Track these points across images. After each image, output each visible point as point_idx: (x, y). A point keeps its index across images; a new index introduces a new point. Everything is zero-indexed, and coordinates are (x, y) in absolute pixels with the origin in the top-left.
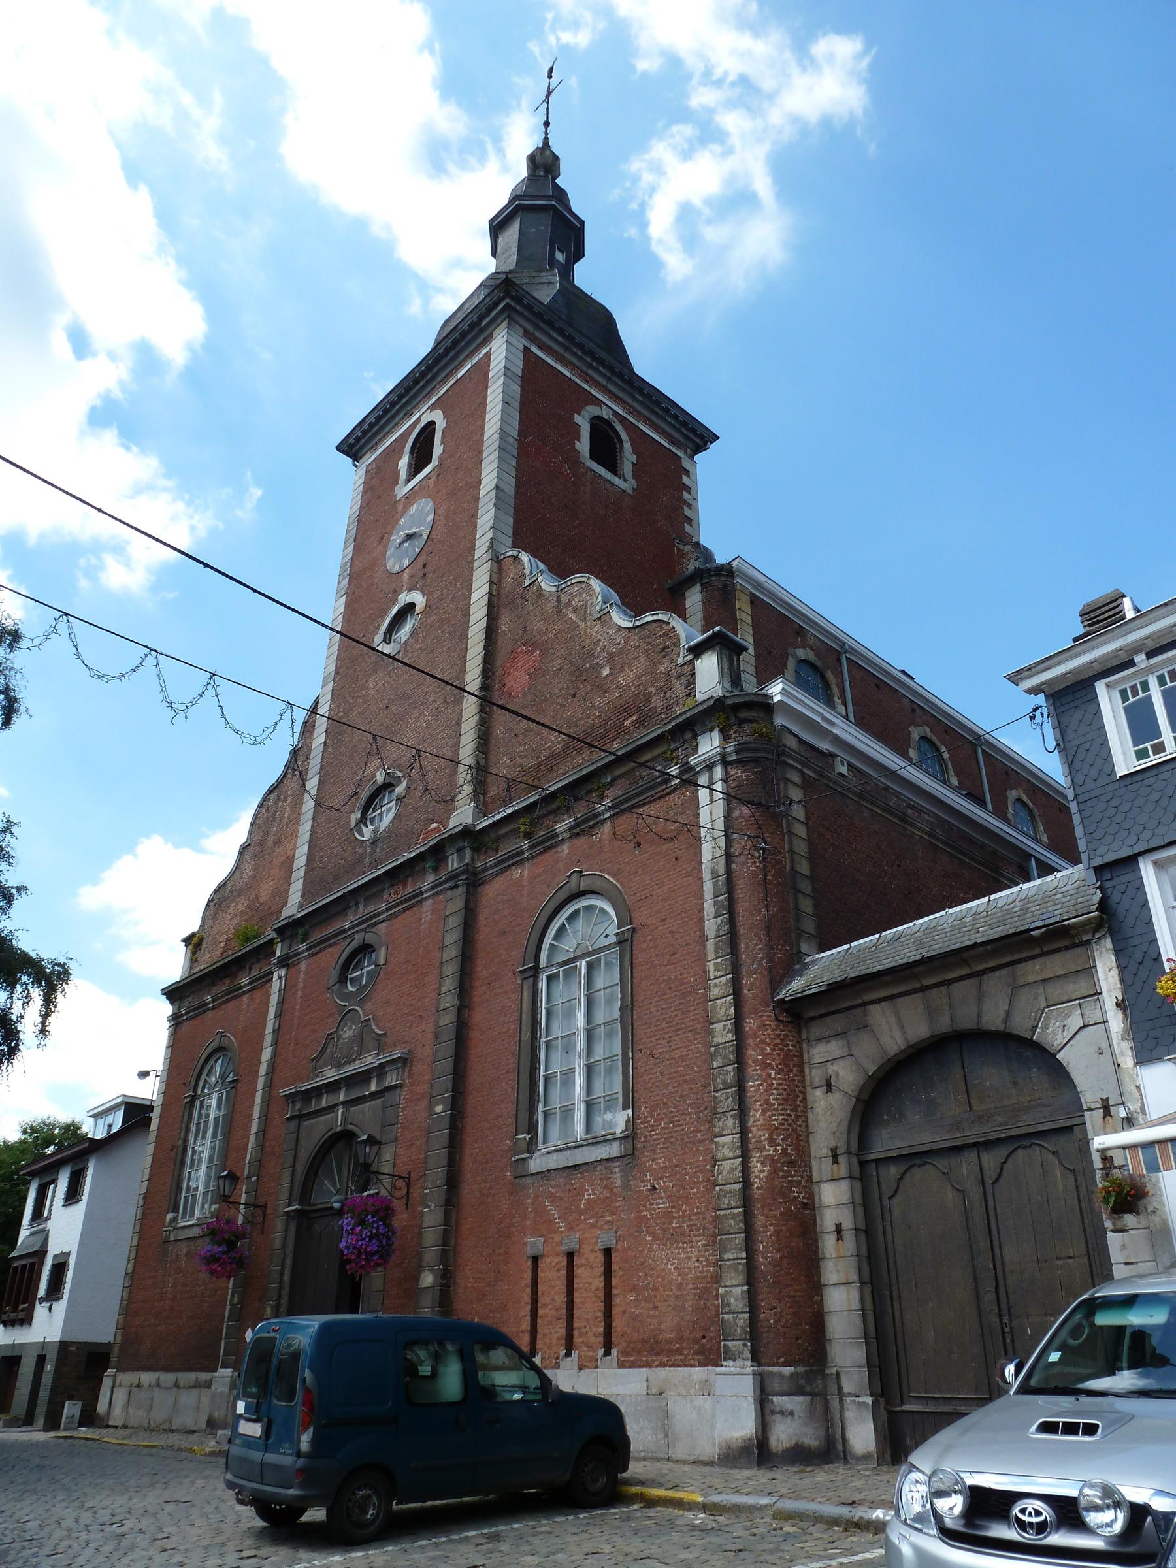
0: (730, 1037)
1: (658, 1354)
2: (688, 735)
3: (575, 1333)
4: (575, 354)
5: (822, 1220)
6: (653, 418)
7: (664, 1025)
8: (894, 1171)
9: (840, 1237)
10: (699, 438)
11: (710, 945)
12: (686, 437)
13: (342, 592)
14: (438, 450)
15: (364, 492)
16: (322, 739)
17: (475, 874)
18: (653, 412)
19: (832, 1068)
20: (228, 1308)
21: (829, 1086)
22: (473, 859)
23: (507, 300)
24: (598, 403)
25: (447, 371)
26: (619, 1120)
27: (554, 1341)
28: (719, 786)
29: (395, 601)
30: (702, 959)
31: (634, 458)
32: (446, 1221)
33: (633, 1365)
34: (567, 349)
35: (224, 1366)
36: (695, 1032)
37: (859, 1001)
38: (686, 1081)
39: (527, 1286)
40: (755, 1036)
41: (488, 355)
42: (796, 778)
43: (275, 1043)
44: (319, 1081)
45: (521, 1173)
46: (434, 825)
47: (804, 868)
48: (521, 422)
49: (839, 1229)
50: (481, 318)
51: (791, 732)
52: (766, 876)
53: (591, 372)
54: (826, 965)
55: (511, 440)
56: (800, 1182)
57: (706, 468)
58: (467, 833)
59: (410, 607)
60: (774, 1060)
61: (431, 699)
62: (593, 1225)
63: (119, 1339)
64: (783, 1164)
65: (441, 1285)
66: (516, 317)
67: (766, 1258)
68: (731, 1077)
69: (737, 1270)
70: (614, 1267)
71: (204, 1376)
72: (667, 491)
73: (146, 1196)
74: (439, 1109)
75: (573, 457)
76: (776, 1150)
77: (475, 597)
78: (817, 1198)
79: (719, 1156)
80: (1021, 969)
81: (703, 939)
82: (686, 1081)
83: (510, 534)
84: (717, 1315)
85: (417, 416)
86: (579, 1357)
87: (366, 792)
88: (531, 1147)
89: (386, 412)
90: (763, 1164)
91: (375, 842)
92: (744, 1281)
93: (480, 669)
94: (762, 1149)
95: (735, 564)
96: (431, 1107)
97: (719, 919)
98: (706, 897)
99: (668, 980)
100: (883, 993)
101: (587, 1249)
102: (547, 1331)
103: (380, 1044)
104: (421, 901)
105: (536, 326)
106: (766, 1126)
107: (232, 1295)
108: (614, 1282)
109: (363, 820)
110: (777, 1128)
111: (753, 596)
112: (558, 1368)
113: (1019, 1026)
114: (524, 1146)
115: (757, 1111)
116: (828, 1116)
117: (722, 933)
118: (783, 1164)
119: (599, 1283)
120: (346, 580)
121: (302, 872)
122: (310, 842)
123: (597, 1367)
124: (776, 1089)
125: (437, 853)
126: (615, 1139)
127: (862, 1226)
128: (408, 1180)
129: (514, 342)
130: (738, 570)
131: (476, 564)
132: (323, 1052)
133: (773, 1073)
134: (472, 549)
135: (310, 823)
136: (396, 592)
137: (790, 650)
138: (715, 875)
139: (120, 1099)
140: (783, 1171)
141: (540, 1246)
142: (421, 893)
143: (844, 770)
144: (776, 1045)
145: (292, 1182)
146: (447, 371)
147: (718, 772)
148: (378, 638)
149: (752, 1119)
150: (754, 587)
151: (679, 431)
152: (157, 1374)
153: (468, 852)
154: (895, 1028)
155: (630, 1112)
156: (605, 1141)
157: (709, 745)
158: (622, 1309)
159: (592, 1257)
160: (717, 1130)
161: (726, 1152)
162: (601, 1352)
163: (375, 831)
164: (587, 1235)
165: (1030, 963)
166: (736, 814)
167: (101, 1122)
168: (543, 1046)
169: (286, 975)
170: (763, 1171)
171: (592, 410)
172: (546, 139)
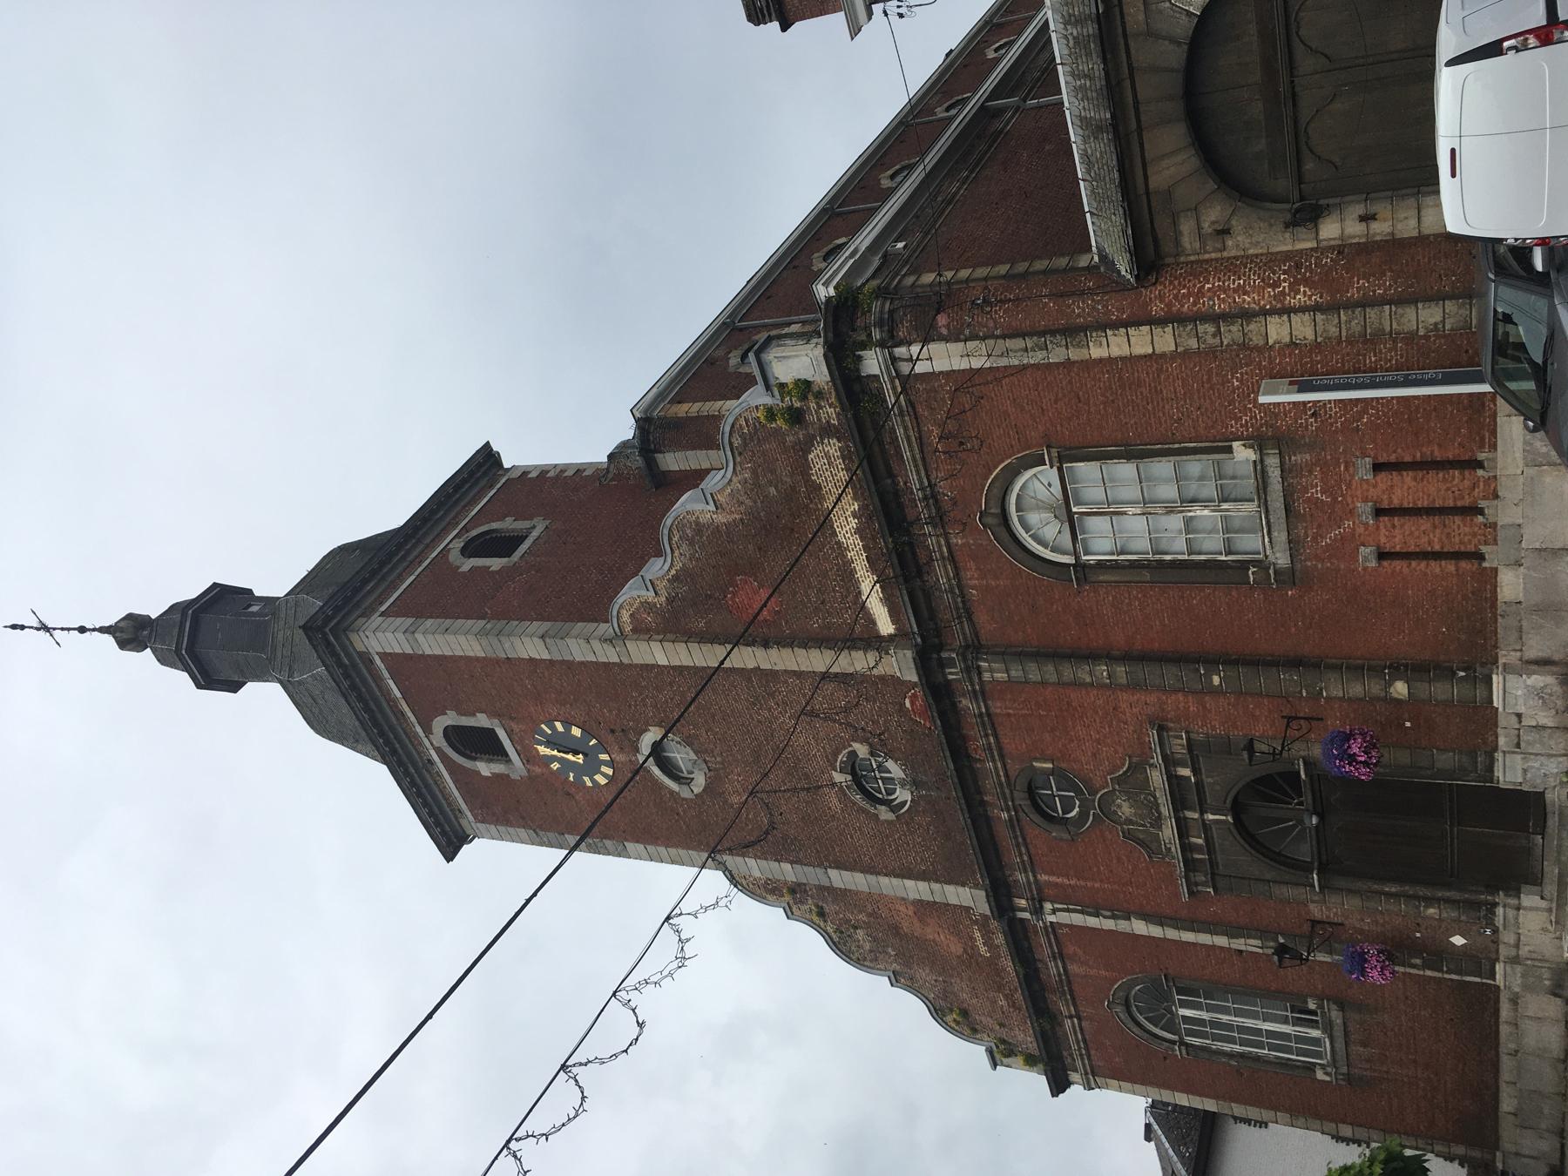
0: (1169, 329)
2: (857, 387)
3: (1459, 504)
8: (1309, 166)
9: (1373, 217)
10: (486, 461)
11: (1075, 354)
12: (485, 474)
14: (482, 721)
15: (508, 823)
16: (787, 867)
17: (967, 647)
20: (1429, 973)
21: (1224, 232)
22: (953, 650)
25: (388, 710)
26: (1243, 454)
28: (915, 349)
30: (1090, 365)
31: (509, 519)
32: (1336, 668)
33: (1494, 433)
34: (383, 578)
35: (1493, 976)
36: (1160, 370)
37: (1144, 198)
38: (1209, 380)
40: (1169, 305)
41: (384, 656)
42: (910, 280)
44: (1176, 849)
45: (1288, 577)
46: (908, 704)
47: (1003, 269)
48: (467, 618)
50: (340, 664)
53: (411, 558)
54: (1104, 233)
62: (1349, 486)
68: (1210, 328)
70: (1393, 458)
71: (1505, 1011)
74: (1216, 680)
77: (662, 660)
80: (1131, 27)
81: (1068, 364)
82: (1209, 380)
84: (1445, 336)
85: (433, 752)
86: (1485, 498)
88: (1262, 565)
94: (1283, 293)
95: (638, 415)
96: (1216, 692)
99: (1104, 403)
100: (1139, 173)
101: (1373, 493)
102: (1457, 540)
103: (1139, 767)
104: (989, 715)
105: (358, 605)
107: (1414, 966)
108: (1408, 459)
111: (672, 402)
112: (1495, 524)
113: (1184, 28)
119: (1408, 477)
121: (936, 886)
122: (903, 877)
126: (1262, 461)
128: (1290, 719)
129: (374, 625)
130: (645, 411)
131: (626, 661)
132: (1142, 843)
134: (607, 666)
137: (731, 370)
142: (981, 714)
146: (388, 710)
147: (901, 351)
151: (478, 480)
152: (1503, 1087)
153: (944, 655)
154: (1172, 161)
155: (1236, 445)
158: (1436, 448)
159: (1382, 486)
161: (1285, 332)
162: (1480, 472)
165: (1128, 19)
166: (944, 331)
168: (1158, 557)
171: (454, 556)
172: (102, 630)
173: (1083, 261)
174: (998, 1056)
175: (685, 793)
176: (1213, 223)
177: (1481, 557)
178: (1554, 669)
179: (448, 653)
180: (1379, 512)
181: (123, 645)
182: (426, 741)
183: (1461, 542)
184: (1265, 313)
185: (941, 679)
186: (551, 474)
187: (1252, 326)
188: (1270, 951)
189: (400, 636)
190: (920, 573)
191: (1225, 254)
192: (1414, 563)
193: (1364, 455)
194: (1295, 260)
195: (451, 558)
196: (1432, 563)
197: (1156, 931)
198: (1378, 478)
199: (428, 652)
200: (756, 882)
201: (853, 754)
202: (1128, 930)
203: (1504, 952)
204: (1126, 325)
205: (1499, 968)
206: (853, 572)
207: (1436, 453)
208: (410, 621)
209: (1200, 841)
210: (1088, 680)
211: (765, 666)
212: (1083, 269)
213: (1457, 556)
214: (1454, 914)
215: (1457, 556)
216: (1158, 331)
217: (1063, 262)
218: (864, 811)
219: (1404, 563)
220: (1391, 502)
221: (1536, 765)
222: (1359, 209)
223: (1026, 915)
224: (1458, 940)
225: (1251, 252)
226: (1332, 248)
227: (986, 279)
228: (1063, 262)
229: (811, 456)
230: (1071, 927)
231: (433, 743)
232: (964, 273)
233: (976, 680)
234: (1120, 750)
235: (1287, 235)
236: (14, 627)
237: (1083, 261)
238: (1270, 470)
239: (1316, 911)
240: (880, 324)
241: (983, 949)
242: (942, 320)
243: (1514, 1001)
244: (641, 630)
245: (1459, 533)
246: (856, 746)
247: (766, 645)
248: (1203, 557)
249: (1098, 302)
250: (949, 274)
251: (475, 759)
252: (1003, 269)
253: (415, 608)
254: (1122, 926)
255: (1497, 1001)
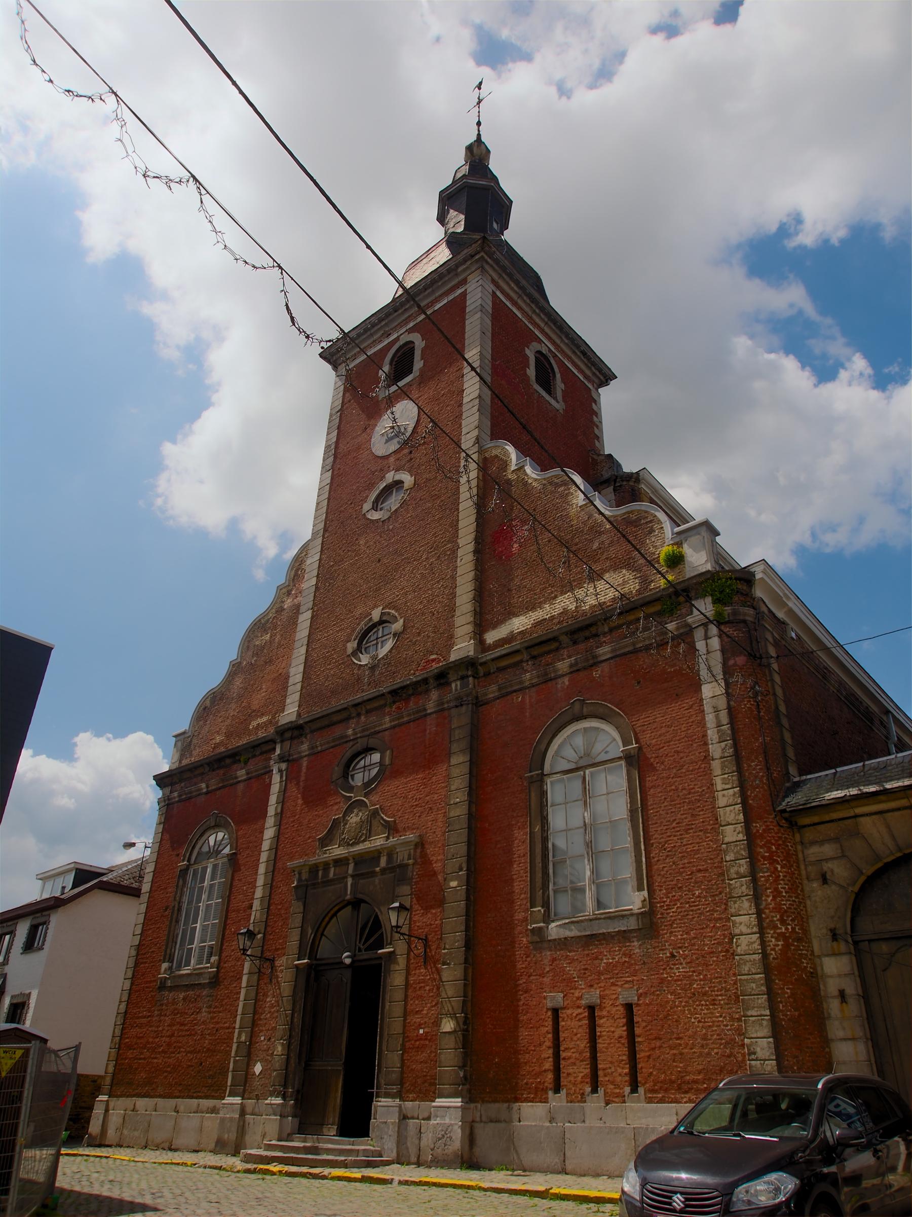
0: (741, 837)
1: (686, 1092)
3: (600, 1073)
4: (525, 301)
5: (825, 986)
6: (573, 357)
7: (674, 824)
8: (884, 947)
10: (606, 377)
11: (716, 765)
12: (594, 374)
13: (328, 468)
14: (418, 364)
18: (574, 352)
19: (827, 866)
20: (235, 1046)
21: (824, 880)
23: (482, 254)
24: (540, 341)
27: (579, 1079)
29: (383, 478)
30: (708, 773)
31: (563, 386)
33: (661, 1101)
34: (520, 296)
35: (232, 1094)
37: (852, 814)
39: (548, 1033)
41: (464, 294)
43: (279, 825)
47: (783, 708)
49: (842, 995)
51: (764, 603)
52: (759, 712)
53: (534, 317)
55: (487, 361)
56: (806, 955)
57: (609, 399)
58: (469, 664)
59: (398, 484)
60: (779, 857)
61: (424, 557)
62: (613, 984)
63: (111, 1069)
64: (794, 940)
65: (464, 1030)
66: (487, 267)
67: (786, 1015)
69: (761, 1025)
71: (210, 1103)
72: (584, 416)
73: (139, 947)
74: (454, 884)
75: (526, 379)
76: (787, 929)
78: (819, 968)
79: (737, 931)
82: (700, 871)
83: (489, 433)
86: (605, 1093)
87: (362, 626)
89: (366, 331)
90: (777, 939)
91: (373, 668)
92: (770, 1034)
93: (473, 536)
94: (775, 927)
95: (641, 473)
97: (723, 744)
98: (709, 725)
101: (607, 1003)
104: (425, 716)
105: (500, 276)
106: (778, 909)
108: (637, 1031)
109: (359, 649)
110: (786, 911)
112: (585, 1102)
114: (540, 917)
115: (768, 896)
116: (824, 905)
117: (726, 754)
118: (794, 940)
119: (622, 1031)
120: (331, 459)
121: (299, 686)
122: (305, 663)
123: (624, 1102)
124: (783, 880)
125: (441, 678)
127: (861, 993)
128: (426, 941)
129: (486, 287)
133: (779, 867)
135: (305, 648)
136: (383, 471)
138: (716, 710)
139: (72, 866)
140: (794, 945)
141: (560, 1000)
143: (793, 635)
144: (779, 845)
145: (301, 940)
147: (713, 630)
148: (367, 506)
149: (764, 903)
150: (653, 492)
151: (590, 368)
156: (623, 916)
157: (705, 606)
160: (733, 910)
161: (744, 929)
162: (627, 1090)
163: (374, 657)
164: (607, 992)
166: (731, 662)
167: (49, 885)
169: (287, 769)
170: (778, 945)
171: (535, 346)
172: (479, 135)
173: (793, 770)
174: (182, 737)
175: (367, 506)
176: (832, 871)
177: (557, 1090)
178: (467, 1148)
179: (467, 336)
180: (591, 1009)
181: (469, 148)
182: (404, 330)
183: (569, 1074)
184: (759, 913)
185: (451, 680)
186: (595, 419)
187: (746, 904)
188: (251, 928)
189: (479, 302)
190: (534, 657)
191: (805, 882)
192: (550, 1036)
193: (640, 996)
194: (804, 937)
195: (534, 344)
196: (551, 1051)
197: (266, 845)
198: (620, 1008)
199: (467, 322)
200: (302, 562)
201: (396, 620)
202: (267, 825)
203: (250, 1103)
204: (744, 803)
205: (237, 1100)
206: (533, 609)
207: (642, 1054)
208: (490, 311)
209: (331, 875)
210: (453, 788)
211: (460, 553)
212: (787, 770)
213: (557, 1070)
214: (277, 1066)
215: (557, 1070)
216: (739, 827)
217: (791, 753)
218: (353, 631)
219: (550, 1028)
220: (601, 1017)
221: (390, 1132)
222: (850, 990)
223: (278, 751)
224: (258, 1068)
225: (808, 902)
226: (815, 968)
227: (775, 694)
228: (791, 753)
229: (624, 571)
230: (270, 784)
231: (402, 335)
232: (777, 679)
233: (452, 704)
234: (400, 814)
235: (824, 931)
236: (481, 83)
237: (793, 770)
238: (625, 921)
239: (281, 962)
240: (735, 613)
241: (254, 724)
242: (741, 660)
243: (214, 1110)
244: (485, 465)
245: (576, 1070)
246: (402, 621)
247: (476, 552)
248: (551, 871)
249: (761, 781)
250: (775, 666)
251: (391, 364)
252: (783, 708)
253: (499, 315)
254: (270, 821)
255: (213, 1098)
